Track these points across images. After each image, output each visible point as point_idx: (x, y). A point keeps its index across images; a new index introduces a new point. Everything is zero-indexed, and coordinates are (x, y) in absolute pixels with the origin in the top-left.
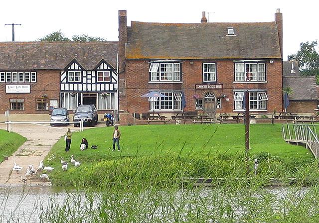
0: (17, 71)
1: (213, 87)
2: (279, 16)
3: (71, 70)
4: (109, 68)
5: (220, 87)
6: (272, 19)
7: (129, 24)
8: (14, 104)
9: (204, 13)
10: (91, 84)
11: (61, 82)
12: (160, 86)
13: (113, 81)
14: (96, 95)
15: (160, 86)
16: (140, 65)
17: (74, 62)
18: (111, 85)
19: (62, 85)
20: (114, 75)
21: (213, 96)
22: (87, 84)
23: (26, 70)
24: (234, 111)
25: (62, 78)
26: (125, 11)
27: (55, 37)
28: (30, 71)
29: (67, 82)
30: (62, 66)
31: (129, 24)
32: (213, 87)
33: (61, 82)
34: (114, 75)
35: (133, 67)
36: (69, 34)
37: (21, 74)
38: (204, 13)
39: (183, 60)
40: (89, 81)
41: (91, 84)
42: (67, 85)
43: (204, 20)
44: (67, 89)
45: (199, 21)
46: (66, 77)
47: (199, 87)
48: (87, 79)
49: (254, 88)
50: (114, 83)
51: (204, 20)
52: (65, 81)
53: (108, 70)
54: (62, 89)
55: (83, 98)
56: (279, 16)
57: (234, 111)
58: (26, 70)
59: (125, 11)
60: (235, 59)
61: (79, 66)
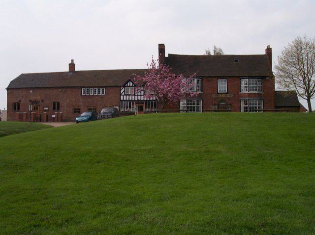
0: (93, 87)
2: (269, 50)
3: (127, 86)
6: (263, 52)
7: (167, 55)
8: (89, 109)
9: (72, 60)
10: (141, 95)
11: (121, 95)
14: (143, 103)
17: (130, 81)
19: (122, 97)
22: (138, 95)
23: (99, 87)
25: (122, 91)
26: (163, 45)
27: (22, 75)
28: (102, 87)
29: (125, 95)
30: (122, 84)
31: (167, 55)
33: (121, 95)
36: (227, 52)
37: (95, 90)
38: (72, 60)
39: (203, 77)
40: (139, 94)
41: (141, 95)
42: (125, 97)
43: (72, 66)
44: (125, 99)
45: (67, 70)
46: (124, 91)
48: (138, 92)
51: (72, 66)
52: (123, 94)
54: (122, 99)
56: (269, 50)
58: (99, 87)
59: (163, 45)
60: (241, 76)
61: (133, 83)
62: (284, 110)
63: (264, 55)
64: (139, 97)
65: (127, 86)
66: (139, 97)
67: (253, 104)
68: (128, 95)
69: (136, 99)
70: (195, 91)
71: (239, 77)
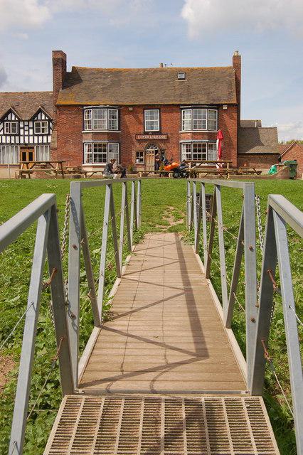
3: (37, 120)
6: (229, 63)
7: (69, 70)
10: (29, 136)
14: (33, 148)
22: (24, 136)
31: (69, 70)
39: (121, 106)
41: (29, 136)
48: (24, 131)
56: (237, 59)
62: (165, 372)
63: (276, 140)
64: (27, 138)
65: (7, 120)
66: (27, 138)
67: (200, 151)
68: (13, 135)
69: (22, 142)
70: (105, 128)
71: (179, 105)
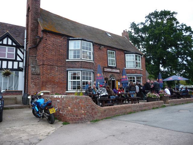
1: (114, 71)
4: (14, 44)
5: (118, 71)
12: (82, 64)
13: (18, 59)
15: (82, 64)
16: (59, 40)
18: (16, 64)
20: (19, 52)
21: (114, 79)
24: (66, 92)
32: (114, 71)
34: (19, 52)
35: (51, 40)
39: (100, 45)
47: (106, 70)
49: (140, 74)
50: (19, 62)
53: (12, 46)
55: (8, 53)
57: (66, 92)
